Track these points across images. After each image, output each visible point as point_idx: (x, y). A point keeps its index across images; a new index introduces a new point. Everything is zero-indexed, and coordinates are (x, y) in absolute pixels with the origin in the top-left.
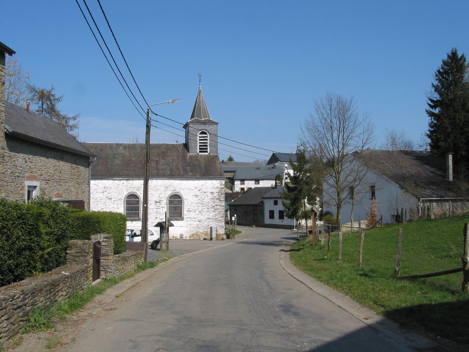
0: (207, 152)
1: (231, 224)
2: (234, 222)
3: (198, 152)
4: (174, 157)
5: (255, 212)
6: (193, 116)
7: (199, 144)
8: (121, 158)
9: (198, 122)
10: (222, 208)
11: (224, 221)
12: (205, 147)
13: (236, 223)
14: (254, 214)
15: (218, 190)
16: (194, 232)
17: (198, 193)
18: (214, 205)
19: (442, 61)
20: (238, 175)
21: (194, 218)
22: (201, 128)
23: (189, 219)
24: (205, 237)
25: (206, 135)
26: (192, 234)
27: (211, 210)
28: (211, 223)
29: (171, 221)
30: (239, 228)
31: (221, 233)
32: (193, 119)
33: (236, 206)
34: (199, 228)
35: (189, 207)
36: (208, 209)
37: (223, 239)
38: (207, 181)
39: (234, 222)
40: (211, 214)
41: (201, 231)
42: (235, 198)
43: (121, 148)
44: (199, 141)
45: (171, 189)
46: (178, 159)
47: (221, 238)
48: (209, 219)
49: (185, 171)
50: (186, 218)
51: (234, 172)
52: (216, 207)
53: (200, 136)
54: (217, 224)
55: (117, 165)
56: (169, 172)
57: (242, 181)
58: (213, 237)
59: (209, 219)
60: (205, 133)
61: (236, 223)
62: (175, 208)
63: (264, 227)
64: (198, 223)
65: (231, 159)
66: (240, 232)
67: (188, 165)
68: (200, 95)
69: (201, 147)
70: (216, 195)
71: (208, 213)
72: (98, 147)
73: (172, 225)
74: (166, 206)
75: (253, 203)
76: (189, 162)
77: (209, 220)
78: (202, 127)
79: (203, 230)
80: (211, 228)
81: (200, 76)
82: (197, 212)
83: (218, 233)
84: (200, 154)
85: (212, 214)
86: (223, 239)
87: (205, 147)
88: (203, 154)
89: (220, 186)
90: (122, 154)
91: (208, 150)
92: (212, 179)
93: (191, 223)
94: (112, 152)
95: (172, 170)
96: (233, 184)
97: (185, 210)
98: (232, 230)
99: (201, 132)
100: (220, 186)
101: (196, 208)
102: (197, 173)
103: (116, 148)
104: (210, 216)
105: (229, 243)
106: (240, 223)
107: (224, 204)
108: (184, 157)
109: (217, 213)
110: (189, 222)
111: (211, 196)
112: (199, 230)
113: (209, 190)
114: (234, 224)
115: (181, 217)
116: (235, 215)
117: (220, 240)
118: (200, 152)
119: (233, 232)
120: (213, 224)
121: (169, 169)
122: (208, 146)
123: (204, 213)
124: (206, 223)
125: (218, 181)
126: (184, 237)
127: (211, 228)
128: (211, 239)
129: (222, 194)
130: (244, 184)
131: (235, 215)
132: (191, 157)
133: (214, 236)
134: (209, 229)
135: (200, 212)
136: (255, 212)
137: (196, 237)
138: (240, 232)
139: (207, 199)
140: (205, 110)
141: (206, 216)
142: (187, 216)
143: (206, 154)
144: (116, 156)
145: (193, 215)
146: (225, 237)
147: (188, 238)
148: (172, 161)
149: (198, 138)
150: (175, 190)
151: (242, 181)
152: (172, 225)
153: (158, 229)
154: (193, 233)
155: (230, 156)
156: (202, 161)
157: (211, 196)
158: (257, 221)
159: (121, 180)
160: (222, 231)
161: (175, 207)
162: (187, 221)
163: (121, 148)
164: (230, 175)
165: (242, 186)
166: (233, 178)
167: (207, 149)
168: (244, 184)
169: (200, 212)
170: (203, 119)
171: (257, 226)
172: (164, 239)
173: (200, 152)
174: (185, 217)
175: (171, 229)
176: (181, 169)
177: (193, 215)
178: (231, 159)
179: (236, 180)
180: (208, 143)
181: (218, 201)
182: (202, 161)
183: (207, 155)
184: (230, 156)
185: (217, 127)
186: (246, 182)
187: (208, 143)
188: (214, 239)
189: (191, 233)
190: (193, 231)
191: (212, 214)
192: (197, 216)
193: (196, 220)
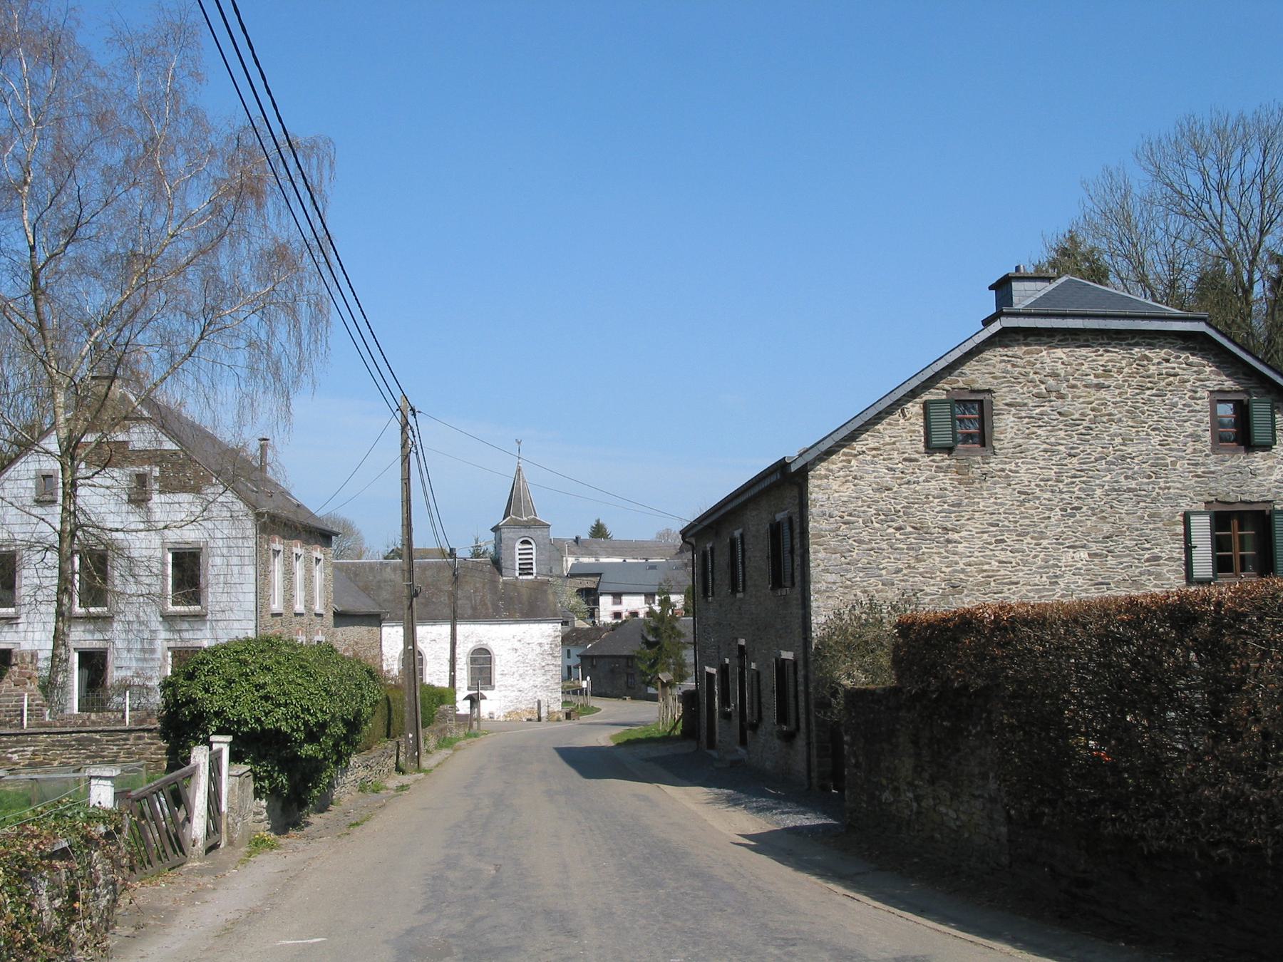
0: (532, 574)
1: (581, 694)
2: (586, 691)
3: (517, 574)
4: (478, 585)
5: (629, 671)
6: (507, 514)
7: (518, 562)
8: (389, 588)
9: (517, 524)
10: (558, 668)
11: (560, 690)
12: (529, 566)
13: (589, 693)
14: (628, 674)
15: (551, 639)
16: (512, 708)
17: (517, 645)
18: (543, 664)
19: (293, 839)
20: (609, 582)
21: (512, 686)
22: (522, 534)
23: (503, 688)
24: (529, 717)
25: (530, 546)
26: (509, 713)
27: (540, 672)
28: (539, 694)
29: (816, 633)
30: (595, 702)
31: (556, 710)
32: (508, 519)
33: (592, 657)
34: (521, 702)
35: (503, 668)
36: (534, 670)
37: (558, 720)
38: (532, 625)
39: (586, 691)
40: (539, 679)
41: (524, 707)
42: (594, 640)
43: (388, 570)
44: (518, 557)
45: (474, 640)
46: (483, 588)
47: (556, 717)
48: (536, 687)
49: (497, 610)
50: (499, 687)
51: (599, 575)
52: (546, 668)
53: (520, 547)
54: (550, 694)
55: (384, 601)
56: (470, 612)
57: (617, 596)
58: (542, 716)
59: (536, 687)
60: (530, 543)
61: (589, 693)
62: (481, 670)
63: (647, 700)
64: (518, 694)
65: (599, 531)
66: (599, 710)
67: (501, 599)
68: (519, 475)
69: (522, 567)
70: (547, 647)
71: (534, 678)
72: (350, 569)
73: (484, 698)
74: (465, 667)
75: (625, 653)
76: (503, 593)
77: (536, 689)
78: (524, 532)
79: (525, 704)
80: (539, 702)
81: (519, 443)
82: (516, 675)
83: (550, 709)
84: (521, 577)
85: (540, 680)
86: (558, 720)
87: (529, 566)
88: (525, 577)
89: (553, 634)
90: (391, 581)
91: (535, 571)
92: (539, 622)
93: (507, 693)
94: (375, 577)
95: (474, 608)
96: (596, 602)
97: (496, 673)
98: (582, 705)
99: (521, 540)
100: (553, 634)
101: (514, 669)
102: (515, 612)
103: (381, 570)
104: (537, 683)
105: (569, 723)
106: (598, 692)
107: (560, 663)
108: (494, 582)
109: (549, 677)
110: (504, 693)
111: (538, 650)
112: (519, 706)
113: (536, 640)
114: (586, 695)
115: (490, 683)
116: (588, 678)
117: (554, 721)
118: (520, 574)
119: (584, 710)
120: (542, 696)
121: (470, 605)
122: (534, 564)
123: (528, 678)
124: (531, 694)
125: (551, 625)
126: (496, 717)
127: (539, 702)
128: (539, 719)
129: (556, 646)
130: (620, 603)
131: (588, 678)
132: (505, 583)
133: (544, 715)
134: (536, 704)
135: (521, 675)
136: (629, 671)
137: (514, 717)
138: (599, 710)
139: (533, 654)
140: (529, 503)
141: (532, 683)
142: (501, 683)
143: (530, 577)
144: (382, 585)
145: (509, 681)
146: (561, 716)
147: (501, 719)
148: (475, 592)
149: (517, 552)
150: (480, 641)
151: (617, 596)
152: (484, 698)
153: (469, 702)
154: (510, 710)
155: (598, 521)
156: (524, 591)
157: (538, 650)
158: (634, 688)
159: (393, 626)
160: (557, 707)
161: (479, 668)
162: (500, 691)
163: (388, 570)
164: (588, 583)
165: (617, 608)
166: (596, 589)
167: (532, 569)
168: (620, 603)
169: (521, 675)
170: (525, 519)
171: (633, 698)
172: (475, 715)
173: (520, 574)
174: (497, 684)
175: (482, 702)
176: (489, 605)
177: (509, 681)
178: (599, 531)
179: (602, 594)
180: (534, 559)
181: (550, 658)
182: (524, 591)
183: (531, 580)
184: (598, 521)
185: (549, 531)
186: (625, 599)
187: (534, 559)
188: (544, 720)
189: (507, 711)
190: (510, 706)
191: (540, 680)
192: (516, 682)
193: (514, 689)
